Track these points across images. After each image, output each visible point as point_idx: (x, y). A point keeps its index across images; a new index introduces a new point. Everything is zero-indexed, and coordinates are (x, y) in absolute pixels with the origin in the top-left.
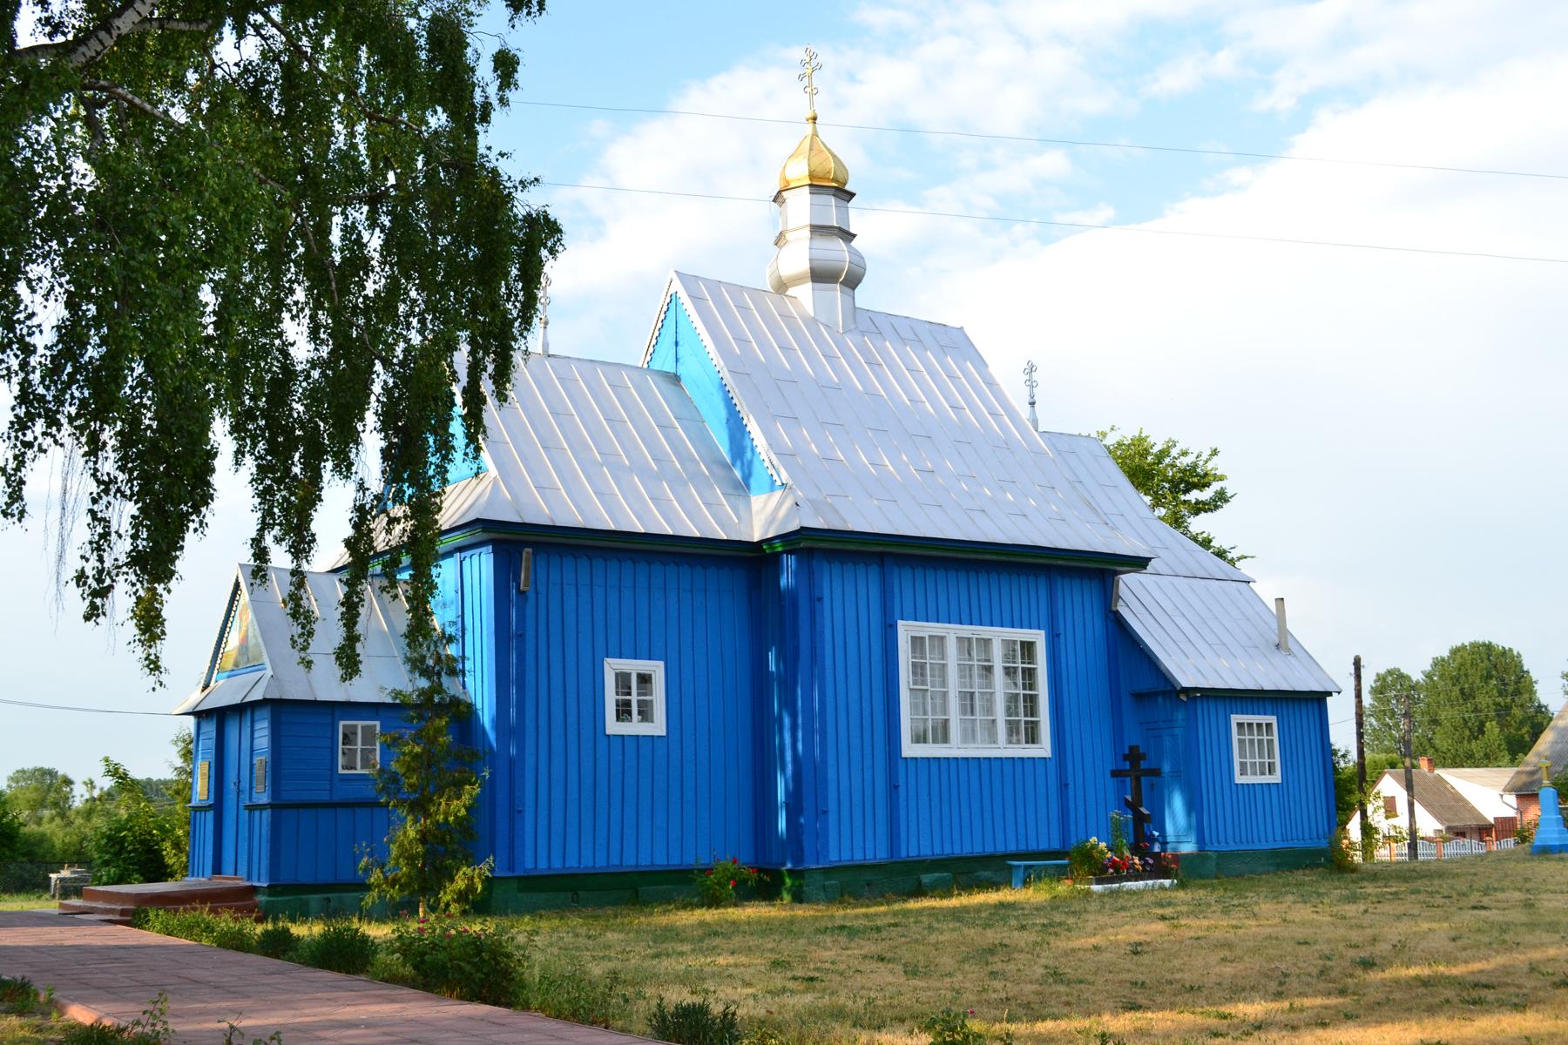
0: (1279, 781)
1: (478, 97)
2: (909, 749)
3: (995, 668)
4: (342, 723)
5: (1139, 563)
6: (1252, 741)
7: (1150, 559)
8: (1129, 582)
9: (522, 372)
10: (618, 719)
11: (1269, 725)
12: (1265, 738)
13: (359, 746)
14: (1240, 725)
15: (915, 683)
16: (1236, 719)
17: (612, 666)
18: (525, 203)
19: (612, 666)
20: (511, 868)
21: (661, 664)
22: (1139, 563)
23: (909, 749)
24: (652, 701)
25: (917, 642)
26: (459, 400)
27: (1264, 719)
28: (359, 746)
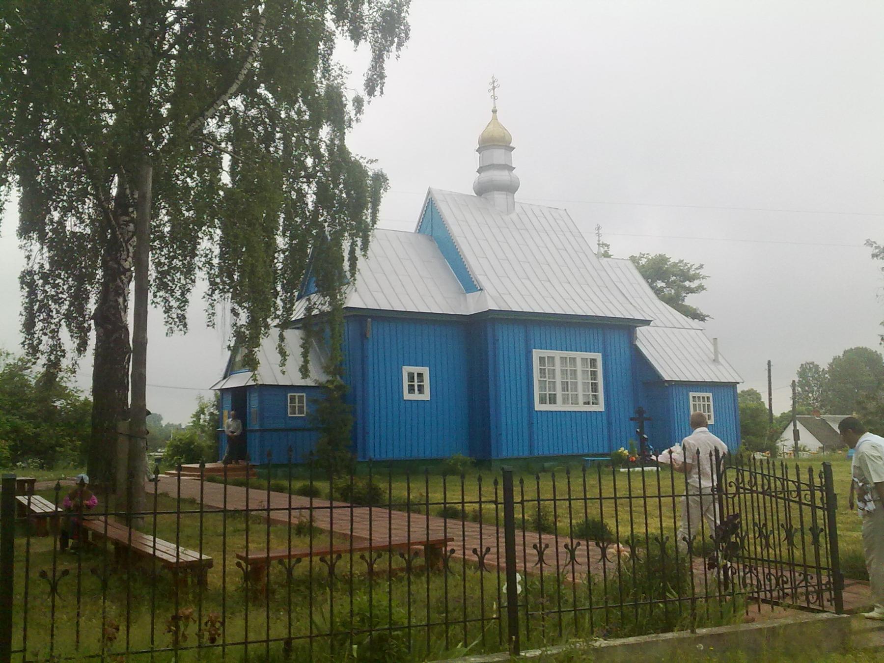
0: (713, 423)
1: (346, 118)
2: (538, 407)
3: (598, 360)
4: (289, 395)
5: (647, 323)
6: (700, 405)
7: (651, 321)
8: (641, 331)
9: (373, 245)
10: (409, 393)
11: (708, 398)
12: (697, 403)
13: (297, 404)
14: (694, 397)
15: (541, 377)
16: (691, 394)
17: (406, 370)
18: (371, 169)
19: (406, 370)
20: (364, 457)
21: (428, 368)
22: (647, 323)
23: (538, 407)
24: (423, 385)
25: (542, 359)
26: (346, 259)
27: (706, 395)
28: (297, 404)
